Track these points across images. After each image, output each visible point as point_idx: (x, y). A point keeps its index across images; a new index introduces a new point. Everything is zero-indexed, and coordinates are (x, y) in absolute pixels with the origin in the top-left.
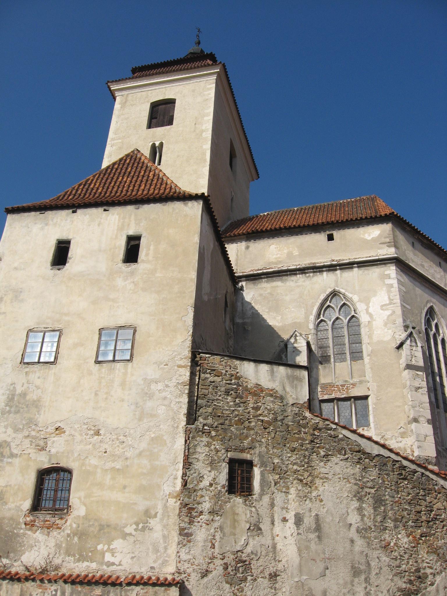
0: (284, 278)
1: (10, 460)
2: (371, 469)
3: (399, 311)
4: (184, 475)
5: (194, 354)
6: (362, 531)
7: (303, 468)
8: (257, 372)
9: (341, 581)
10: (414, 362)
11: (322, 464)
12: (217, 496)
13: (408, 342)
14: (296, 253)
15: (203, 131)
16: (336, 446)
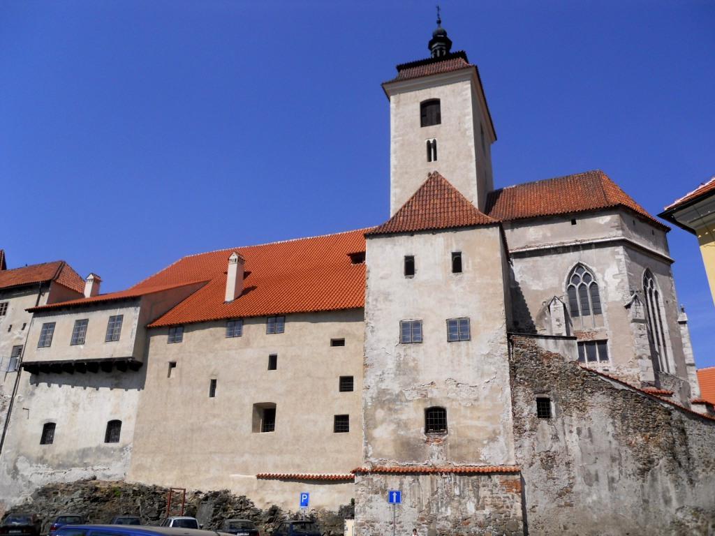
1: (406, 404)
3: (626, 279)
4: (513, 409)
5: (509, 335)
6: (616, 436)
8: (547, 343)
9: (606, 465)
10: (638, 317)
12: (533, 421)
13: (634, 303)
14: (549, 234)
15: (466, 130)
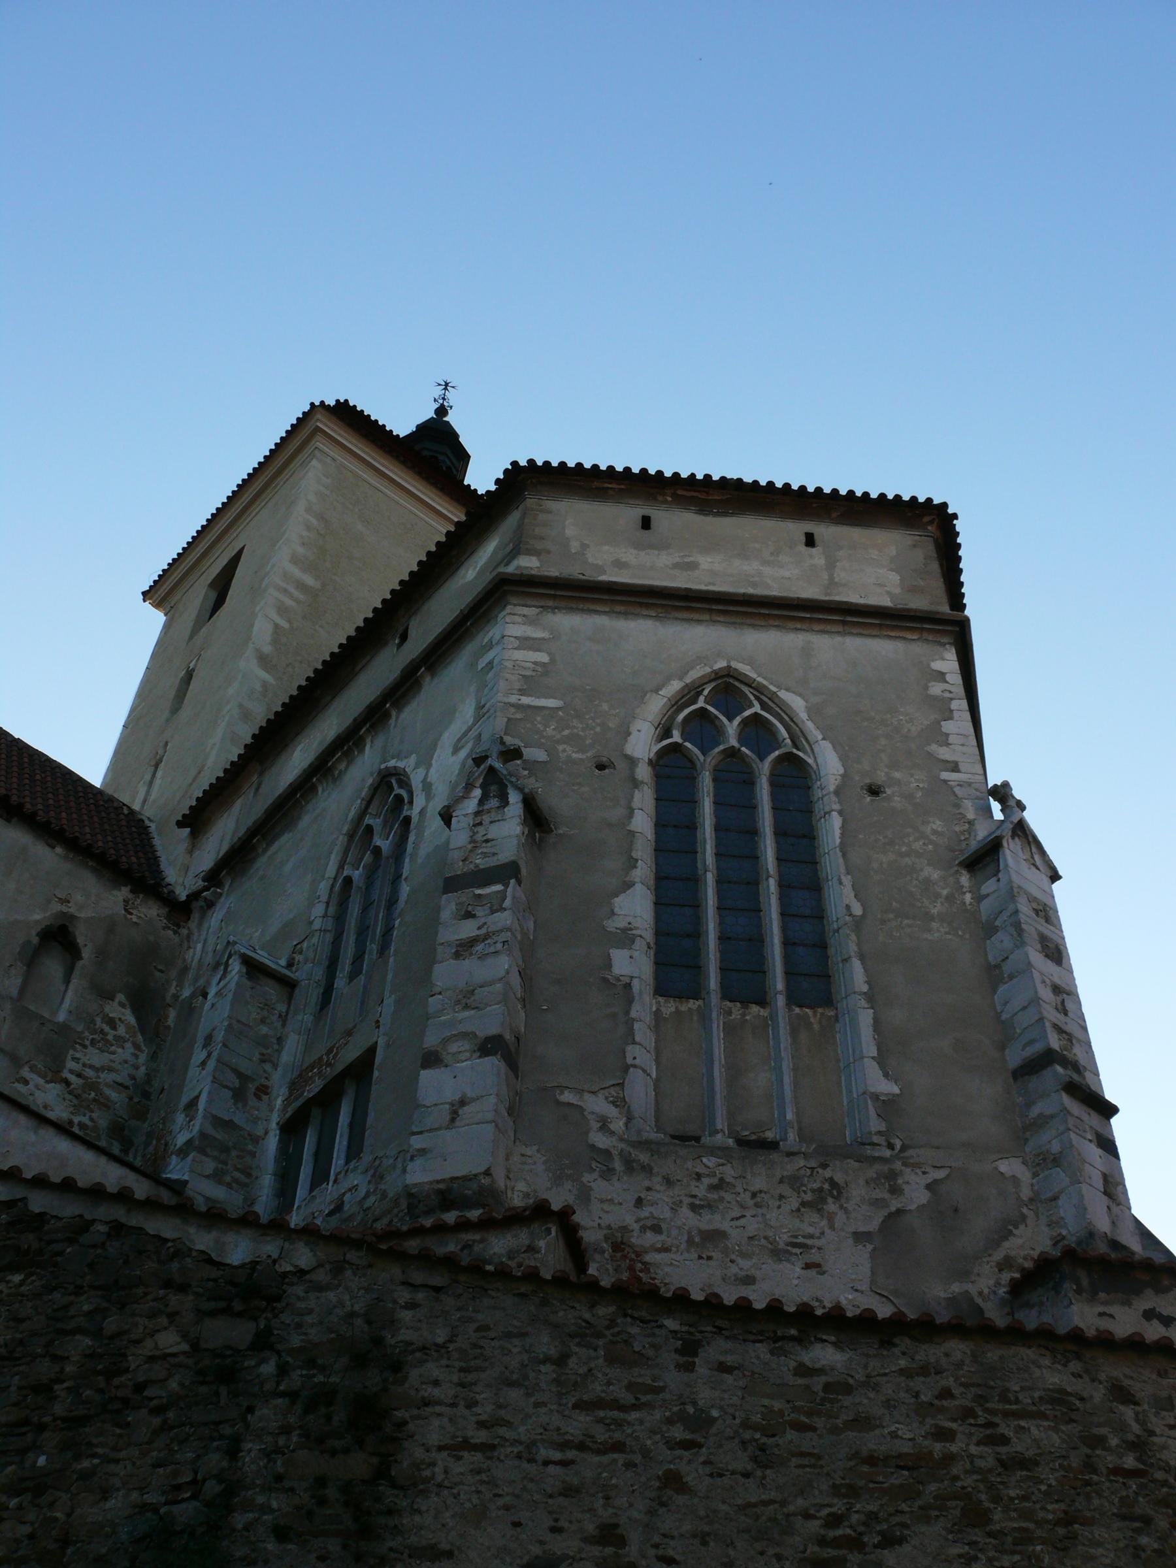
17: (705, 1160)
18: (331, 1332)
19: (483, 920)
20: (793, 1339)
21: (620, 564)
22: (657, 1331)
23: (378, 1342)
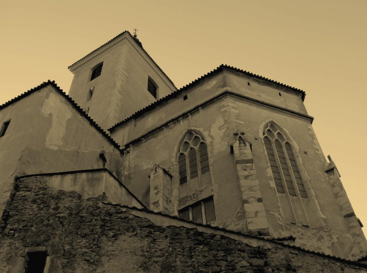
0: (156, 134)
2: (161, 240)
7: (91, 249)
11: (110, 243)
16: (125, 226)
17: (299, 229)
18: (280, 263)
19: (249, 171)
20: (358, 269)
21: (247, 93)
22: (336, 265)
23: (290, 265)
